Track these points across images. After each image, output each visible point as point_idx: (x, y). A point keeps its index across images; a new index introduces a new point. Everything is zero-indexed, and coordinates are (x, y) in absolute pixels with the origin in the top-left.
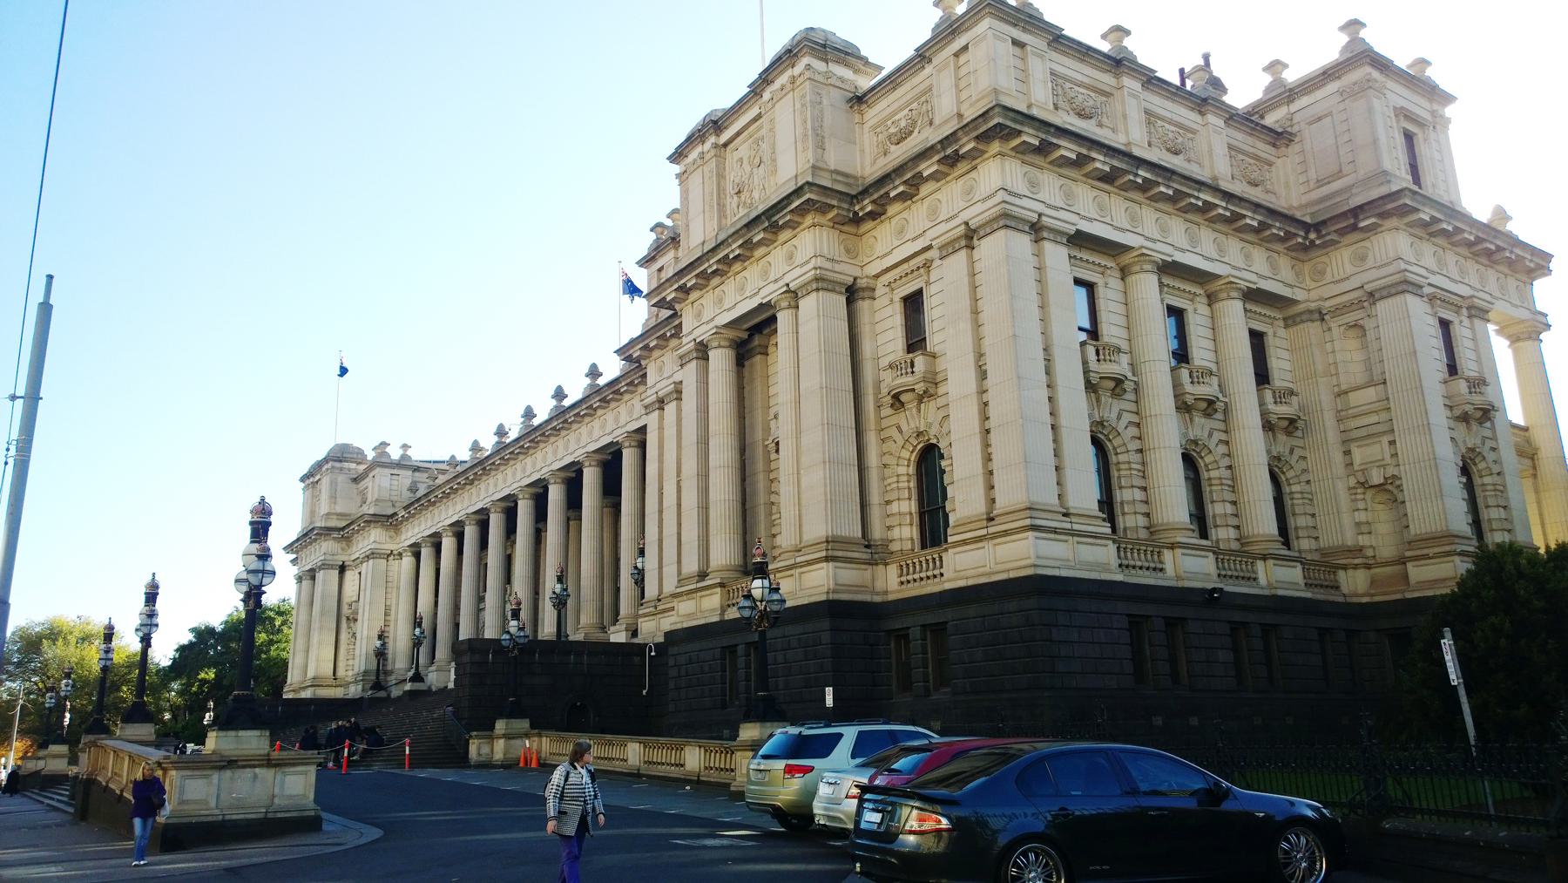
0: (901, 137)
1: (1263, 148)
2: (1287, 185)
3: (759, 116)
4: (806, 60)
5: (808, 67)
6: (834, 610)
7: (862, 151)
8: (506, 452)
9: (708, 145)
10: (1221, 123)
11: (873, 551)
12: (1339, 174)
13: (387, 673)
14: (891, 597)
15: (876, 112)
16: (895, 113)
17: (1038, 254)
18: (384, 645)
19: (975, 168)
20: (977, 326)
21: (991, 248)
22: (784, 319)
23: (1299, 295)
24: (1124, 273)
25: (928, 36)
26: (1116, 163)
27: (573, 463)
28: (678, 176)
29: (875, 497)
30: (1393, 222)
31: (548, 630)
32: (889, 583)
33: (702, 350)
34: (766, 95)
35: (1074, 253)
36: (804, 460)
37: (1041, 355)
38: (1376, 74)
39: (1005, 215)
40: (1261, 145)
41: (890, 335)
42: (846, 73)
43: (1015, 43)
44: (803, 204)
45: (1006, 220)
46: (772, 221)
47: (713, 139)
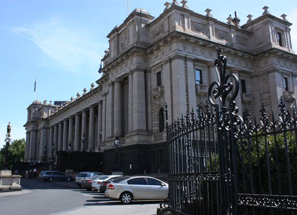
0: (158, 34)
1: (246, 36)
2: (251, 45)
3: (126, 29)
4: (136, 16)
5: (136, 18)
6: (138, 146)
7: (149, 37)
8: (80, 100)
9: (134, 18)
10: (234, 31)
11: (149, 132)
12: (262, 43)
13: (47, 157)
14: (152, 143)
15: (152, 28)
16: (156, 29)
17: (186, 64)
18: (46, 150)
19: (171, 44)
20: (171, 80)
21: (175, 63)
22: (130, 77)
23: (253, 71)
24: (209, 67)
25: (163, 12)
26: (205, 43)
27: (96, 103)
28: (109, 41)
29: (150, 120)
30: (272, 55)
31: (76, 149)
32: (152, 140)
33: (113, 84)
34: (127, 24)
35: (195, 63)
36: (134, 111)
37: (185, 88)
38: (270, 19)
39: (177, 56)
40: (245, 35)
41: (154, 82)
42: (146, 19)
43: (181, 15)
44: (137, 47)
45: (178, 57)
46: (127, 54)
47: (116, 33)
